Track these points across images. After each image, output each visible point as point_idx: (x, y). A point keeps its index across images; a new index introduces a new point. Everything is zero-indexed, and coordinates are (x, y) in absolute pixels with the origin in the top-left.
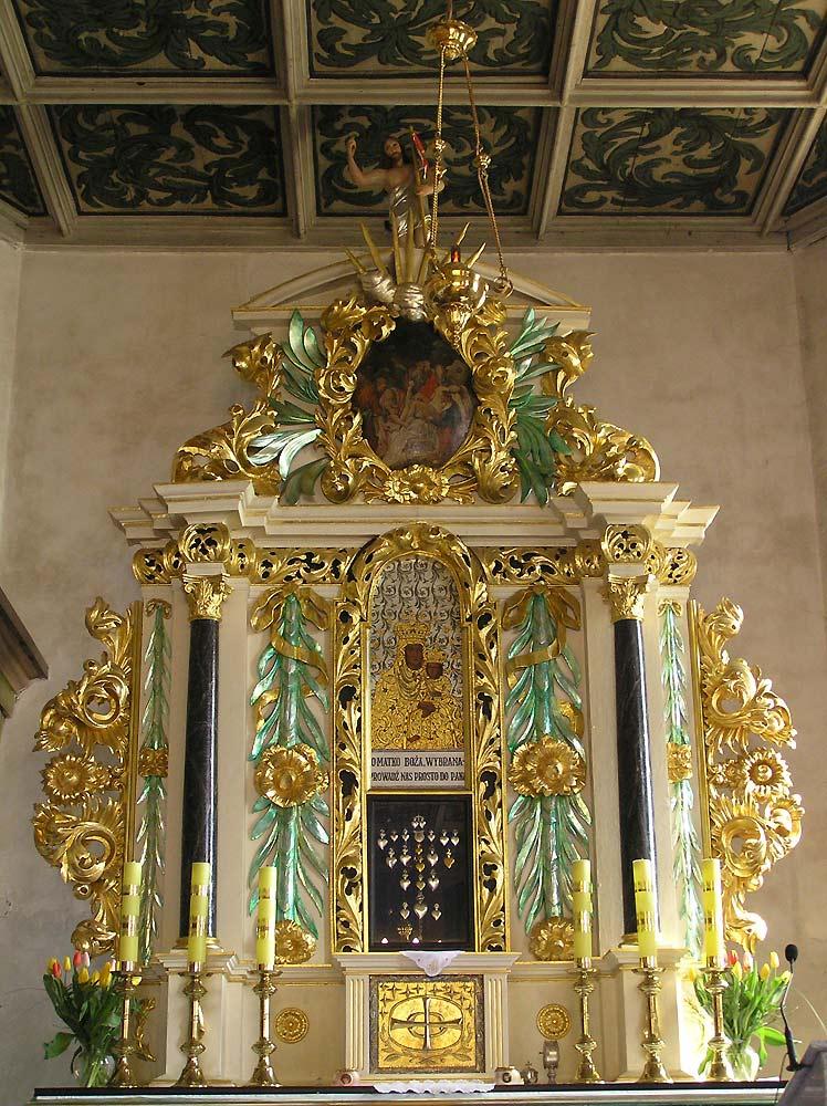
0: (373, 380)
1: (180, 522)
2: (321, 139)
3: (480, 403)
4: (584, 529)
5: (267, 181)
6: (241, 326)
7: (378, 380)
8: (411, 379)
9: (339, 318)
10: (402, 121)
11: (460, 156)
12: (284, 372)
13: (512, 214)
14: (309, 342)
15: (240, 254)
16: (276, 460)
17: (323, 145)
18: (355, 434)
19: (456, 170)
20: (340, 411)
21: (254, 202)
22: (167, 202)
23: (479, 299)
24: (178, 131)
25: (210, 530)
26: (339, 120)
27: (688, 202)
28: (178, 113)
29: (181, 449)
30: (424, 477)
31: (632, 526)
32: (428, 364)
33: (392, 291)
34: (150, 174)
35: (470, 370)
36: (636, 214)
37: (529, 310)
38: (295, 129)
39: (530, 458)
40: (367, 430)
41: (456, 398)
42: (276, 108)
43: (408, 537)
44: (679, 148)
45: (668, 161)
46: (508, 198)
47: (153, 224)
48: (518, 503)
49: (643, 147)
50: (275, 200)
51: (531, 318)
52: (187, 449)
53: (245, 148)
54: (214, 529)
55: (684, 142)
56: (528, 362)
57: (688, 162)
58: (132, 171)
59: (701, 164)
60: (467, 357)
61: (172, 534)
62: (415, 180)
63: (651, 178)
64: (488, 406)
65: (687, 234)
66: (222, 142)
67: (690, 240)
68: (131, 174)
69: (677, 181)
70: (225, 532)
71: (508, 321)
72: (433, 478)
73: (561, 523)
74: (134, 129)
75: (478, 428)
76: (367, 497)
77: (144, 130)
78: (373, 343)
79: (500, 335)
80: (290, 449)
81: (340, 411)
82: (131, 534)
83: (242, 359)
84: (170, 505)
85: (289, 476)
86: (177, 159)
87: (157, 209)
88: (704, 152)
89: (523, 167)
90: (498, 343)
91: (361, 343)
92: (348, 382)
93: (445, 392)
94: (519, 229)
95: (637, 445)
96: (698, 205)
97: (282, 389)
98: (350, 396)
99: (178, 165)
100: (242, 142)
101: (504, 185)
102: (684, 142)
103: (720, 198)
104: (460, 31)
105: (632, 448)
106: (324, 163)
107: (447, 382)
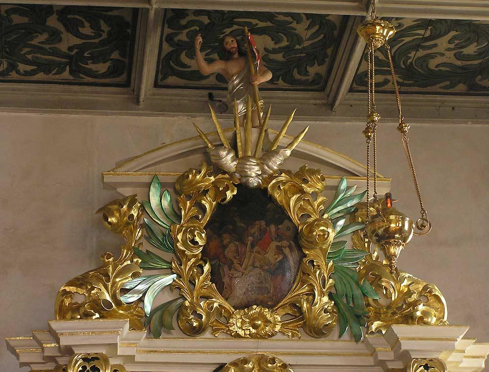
0: (220, 235)
1: (69, 351)
2: (167, 31)
3: (305, 256)
4: (392, 361)
5: (119, 60)
6: (112, 186)
7: (224, 235)
8: (248, 231)
9: (192, 184)
10: (235, 20)
11: (277, 46)
12: (144, 226)
13: (311, 90)
14: (166, 203)
15: (89, 116)
16: (141, 300)
17: (168, 36)
18: (205, 279)
19: (272, 56)
20: (193, 260)
21: (104, 76)
22: (33, 73)
23: (409, 236)
24: (53, 22)
25: (93, 359)
26: (185, 18)
27: (452, 86)
28: (55, 9)
29: (62, 288)
30: (261, 316)
31: (431, 360)
32: (263, 223)
33: (235, 163)
34: (22, 53)
35: (296, 228)
36: (412, 93)
37: (342, 180)
38: (151, 25)
39: (345, 300)
40: (215, 276)
41: (287, 251)
42: (135, 11)
43: (250, 366)
44: (452, 46)
45: (442, 55)
46: (310, 78)
47: (20, 90)
48: (336, 338)
49: (423, 44)
50: (123, 77)
51: (344, 185)
52: (68, 289)
53: (105, 36)
54: (97, 359)
55: (457, 42)
56: (341, 222)
57: (458, 56)
58: (7, 49)
59: (468, 57)
60: (295, 219)
61: (58, 359)
62: (249, 71)
63: (427, 67)
64: (312, 258)
65: (451, 108)
66: (87, 30)
67: (454, 114)
68: (6, 52)
69: (448, 69)
70: (106, 361)
71: (326, 188)
72: (268, 316)
73: (372, 355)
74: (17, 19)
75: (304, 272)
76: (215, 331)
77: (25, 20)
78: (218, 204)
79: (320, 199)
80: (151, 290)
81: (193, 260)
82: (23, 359)
83: (113, 215)
84: (61, 338)
85: (153, 312)
86: (47, 42)
87: (23, 78)
88: (471, 49)
89: (326, 55)
90: (318, 206)
91: (208, 203)
92: (201, 237)
93: (277, 247)
94: (318, 102)
95: (430, 292)
96: (461, 87)
97: (143, 240)
98: (201, 248)
99: (47, 47)
100: (103, 32)
101: (309, 68)
102: (457, 42)
103: (480, 83)
104: (383, 28)
105: (426, 293)
106: (167, 48)
107: (279, 238)
